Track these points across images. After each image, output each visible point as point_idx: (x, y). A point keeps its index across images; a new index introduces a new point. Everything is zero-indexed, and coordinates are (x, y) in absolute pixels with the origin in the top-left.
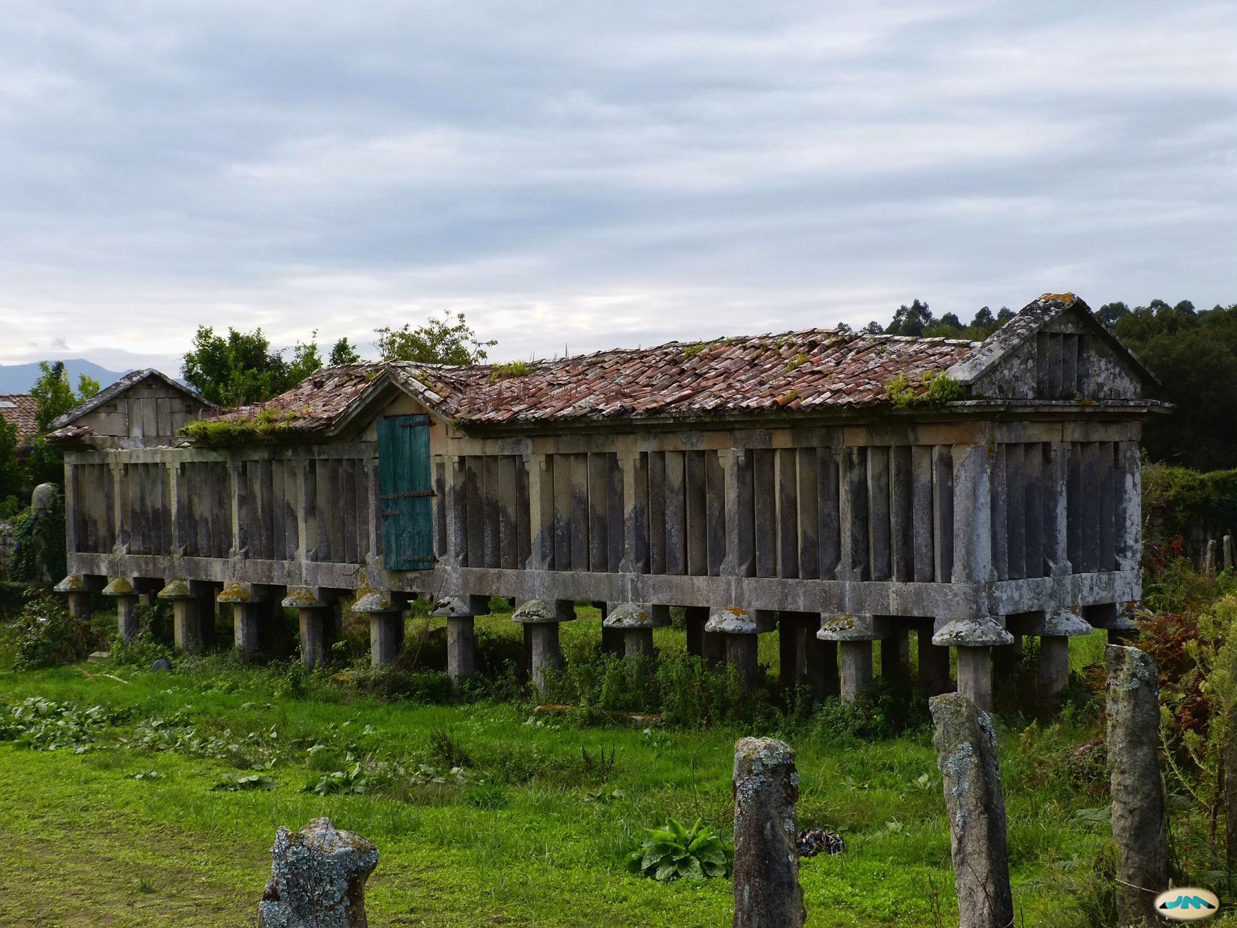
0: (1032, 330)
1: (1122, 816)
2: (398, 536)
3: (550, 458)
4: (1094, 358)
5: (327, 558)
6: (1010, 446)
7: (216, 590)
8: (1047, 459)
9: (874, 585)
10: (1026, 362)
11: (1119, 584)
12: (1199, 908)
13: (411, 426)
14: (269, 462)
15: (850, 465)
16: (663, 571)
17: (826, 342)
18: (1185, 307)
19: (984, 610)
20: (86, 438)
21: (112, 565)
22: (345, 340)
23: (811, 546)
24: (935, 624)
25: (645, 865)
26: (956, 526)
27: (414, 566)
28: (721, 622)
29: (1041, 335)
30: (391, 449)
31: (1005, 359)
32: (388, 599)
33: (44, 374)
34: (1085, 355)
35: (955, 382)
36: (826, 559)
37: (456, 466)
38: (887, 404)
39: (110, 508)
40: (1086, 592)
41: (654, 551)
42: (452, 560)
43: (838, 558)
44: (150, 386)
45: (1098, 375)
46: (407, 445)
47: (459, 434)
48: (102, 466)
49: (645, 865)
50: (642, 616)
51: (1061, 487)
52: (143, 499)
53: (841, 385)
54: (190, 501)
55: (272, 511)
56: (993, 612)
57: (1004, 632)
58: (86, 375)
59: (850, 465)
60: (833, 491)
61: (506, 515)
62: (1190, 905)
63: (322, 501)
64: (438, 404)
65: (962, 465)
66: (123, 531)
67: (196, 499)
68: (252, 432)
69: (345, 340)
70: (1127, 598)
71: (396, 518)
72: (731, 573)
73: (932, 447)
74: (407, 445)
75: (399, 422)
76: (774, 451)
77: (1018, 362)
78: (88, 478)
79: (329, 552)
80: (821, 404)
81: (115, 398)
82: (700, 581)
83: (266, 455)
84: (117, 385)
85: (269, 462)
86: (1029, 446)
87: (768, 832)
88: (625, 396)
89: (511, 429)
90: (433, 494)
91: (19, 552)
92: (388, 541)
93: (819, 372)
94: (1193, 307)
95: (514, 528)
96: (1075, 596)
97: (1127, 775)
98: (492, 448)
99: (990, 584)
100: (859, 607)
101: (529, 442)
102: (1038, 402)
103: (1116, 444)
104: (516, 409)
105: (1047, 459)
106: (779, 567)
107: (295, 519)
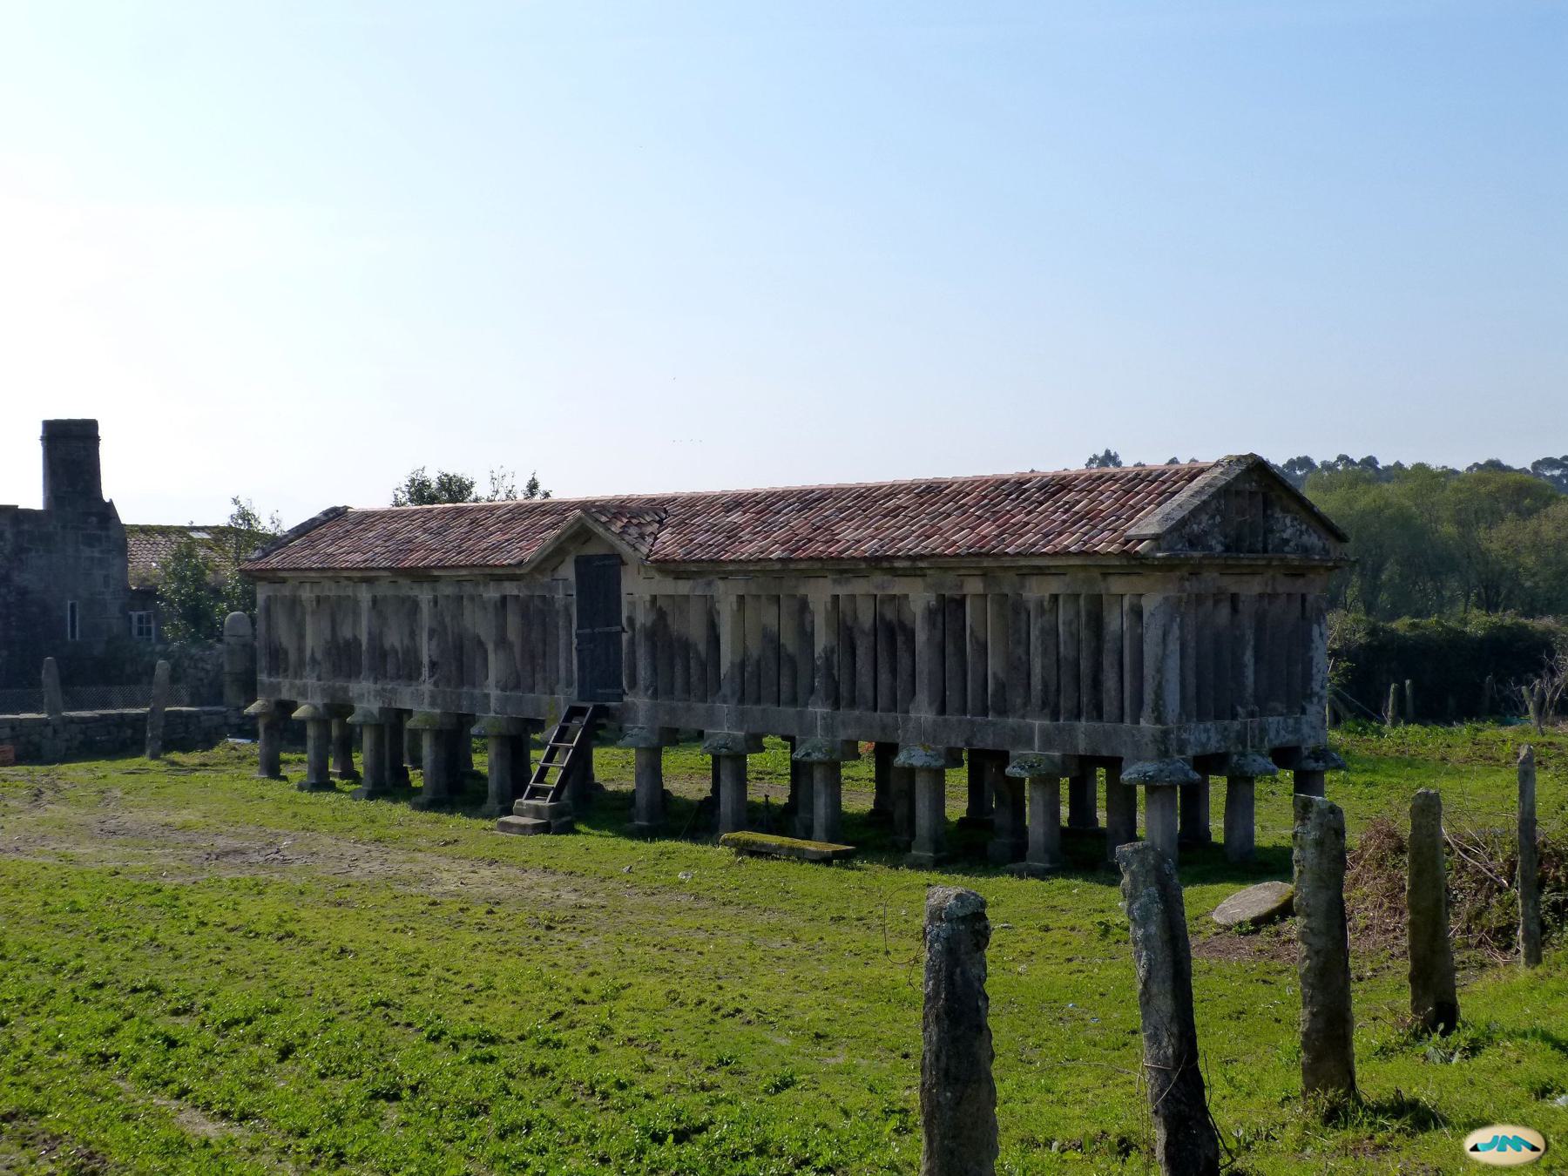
1: (1307, 957)
3: (741, 598)
4: (1279, 514)
7: (405, 716)
8: (1235, 609)
10: (1213, 517)
12: (1519, 1150)
18: (1370, 462)
23: (1001, 687)
24: (1123, 764)
26: (1145, 671)
28: (910, 758)
34: (1269, 512)
37: (648, 605)
40: (1272, 734)
41: (844, 690)
45: (1284, 531)
55: (461, 648)
57: (1191, 772)
62: (1508, 1146)
63: (513, 634)
77: (1207, 517)
87: (958, 978)
94: (1377, 463)
95: (703, 666)
97: (1313, 918)
98: (683, 587)
102: (1225, 555)
105: (1235, 609)
107: (486, 652)
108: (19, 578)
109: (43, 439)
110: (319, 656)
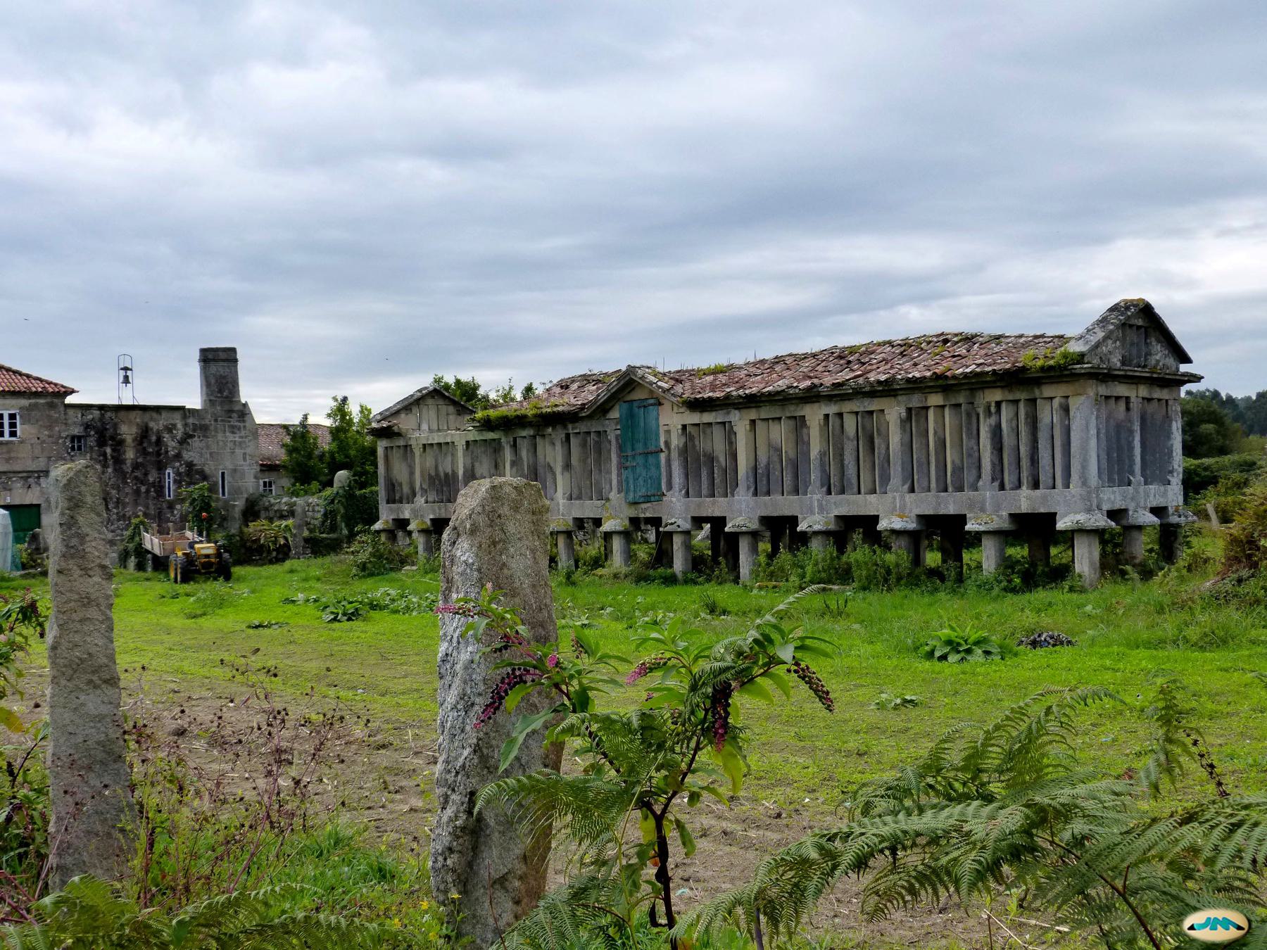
0: (1120, 320)
2: (636, 480)
3: (753, 422)
5: (579, 498)
6: (1107, 398)
9: (1008, 493)
10: (1115, 342)
11: (1170, 494)
12: (1228, 929)
13: (645, 407)
14: (534, 437)
15: (988, 413)
16: (843, 492)
17: (955, 339)
19: (1094, 507)
20: (395, 429)
21: (414, 511)
22: (531, 384)
23: (958, 470)
25: (937, 654)
26: (1072, 450)
27: (647, 499)
29: (1124, 326)
30: (630, 422)
31: (1106, 338)
32: (627, 522)
33: (335, 404)
35: (1074, 353)
36: (968, 477)
37: (680, 431)
38: (1024, 369)
39: (412, 473)
40: (1151, 498)
42: (677, 494)
43: (979, 477)
44: (433, 397)
46: (642, 419)
47: (682, 410)
48: (406, 446)
49: (937, 654)
50: (826, 523)
51: (1137, 427)
52: (436, 467)
53: (982, 361)
54: (473, 466)
55: (536, 470)
56: (1099, 508)
58: (364, 404)
59: (988, 413)
60: (975, 432)
61: (718, 461)
64: (668, 390)
65: (1078, 409)
66: (422, 488)
67: (477, 465)
68: (525, 416)
69: (531, 384)
70: (1175, 504)
71: (634, 468)
72: (896, 491)
73: (1051, 399)
74: (642, 419)
75: (635, 404)
76: (927, 408)
78: (396, 456)
79: (581, 493)
80: (971, 372)
81: (411, 404)
82: (872, 498)
83: (532, 432)
84: (412, 396)
85: (534, 437)
86: (1118, 398)
88: (810, 378)
89: (726, 403)
90: (662, 451)
91: (325, 515)
92: (628, 483)
93: (959, 355)
96: (1146, 500)
98: (708, 417)
99: (1097, 489)
100: (997, 508)
101: (737, 412)
103: (1167, 401)
104: (728, 390)
105: (1128, 409)
106: (933, 485)
107: (554, 474)
108: (187, 456)
109: (200, 361)
110: (425, 486)
